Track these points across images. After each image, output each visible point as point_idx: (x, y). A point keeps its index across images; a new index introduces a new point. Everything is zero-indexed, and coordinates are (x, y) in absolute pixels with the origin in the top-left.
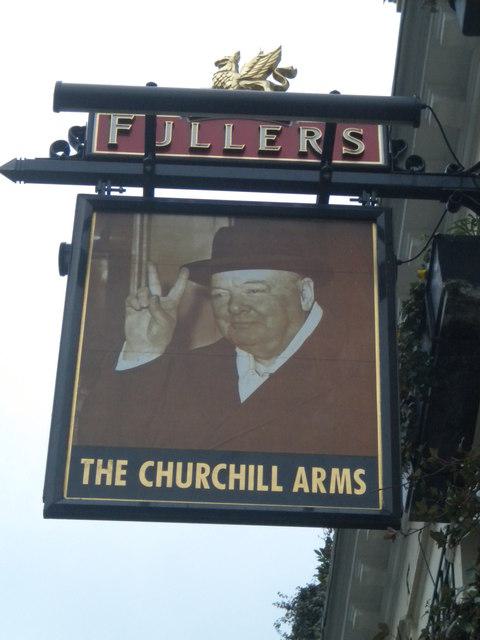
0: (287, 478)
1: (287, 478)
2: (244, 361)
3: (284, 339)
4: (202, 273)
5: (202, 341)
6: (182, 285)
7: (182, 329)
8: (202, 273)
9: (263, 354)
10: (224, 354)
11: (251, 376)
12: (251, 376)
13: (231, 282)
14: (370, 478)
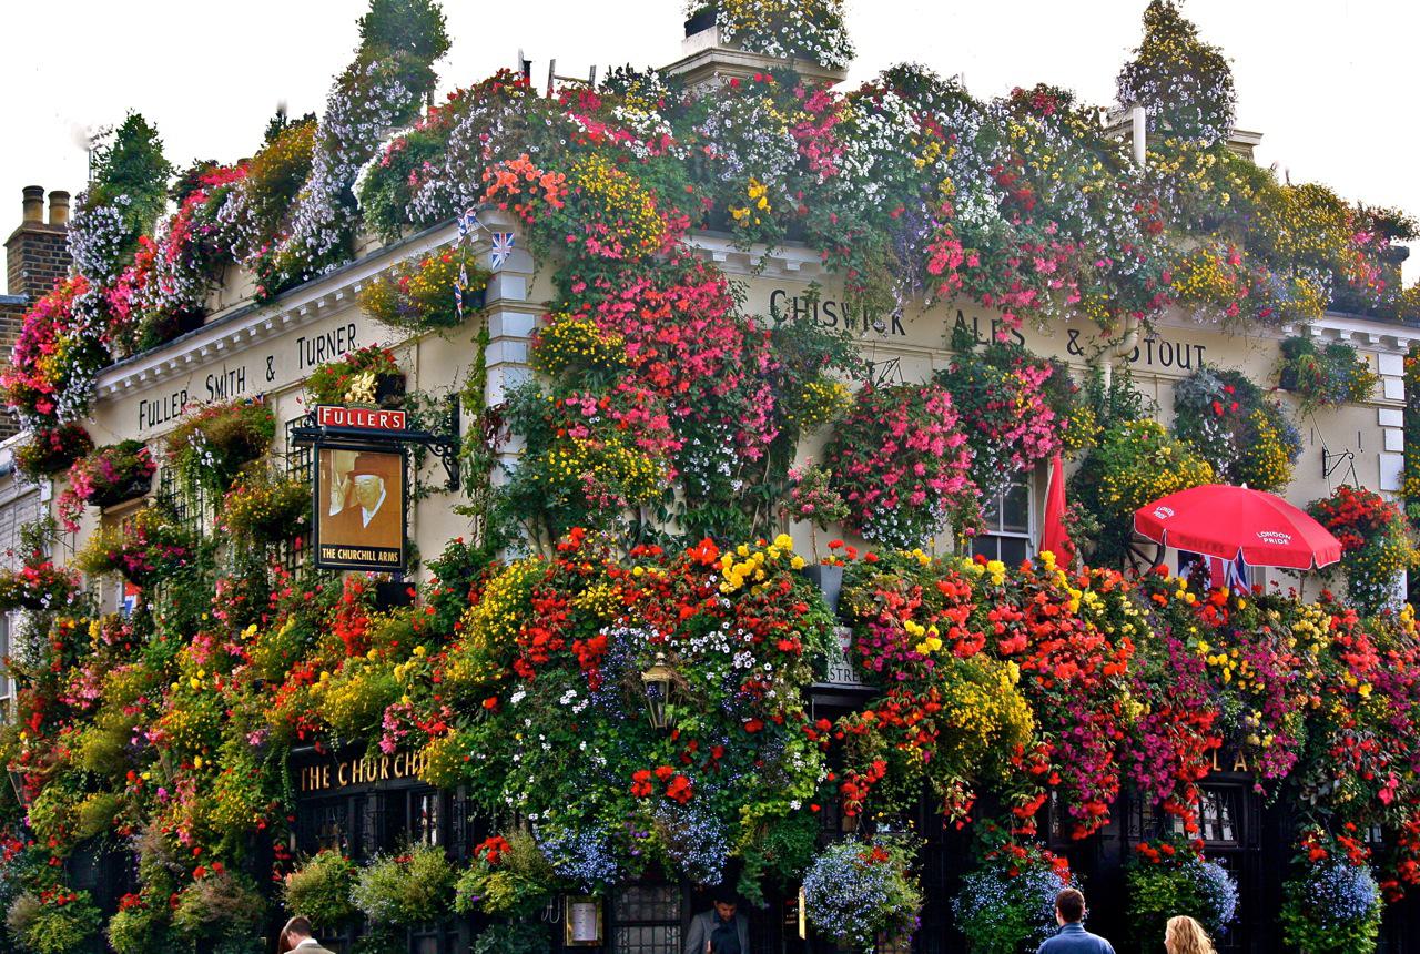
0: (377, 557)
1: (377, 557)
3: (375, 503)
4: (352, 476)
5: (352, 505)
6: (346, 481)
7: (347, 499)
8: (352, 476)
10: (358, 509)
11: (367, 516)
12: (367, 516)
13: (360, 479)
14: (399, 556)
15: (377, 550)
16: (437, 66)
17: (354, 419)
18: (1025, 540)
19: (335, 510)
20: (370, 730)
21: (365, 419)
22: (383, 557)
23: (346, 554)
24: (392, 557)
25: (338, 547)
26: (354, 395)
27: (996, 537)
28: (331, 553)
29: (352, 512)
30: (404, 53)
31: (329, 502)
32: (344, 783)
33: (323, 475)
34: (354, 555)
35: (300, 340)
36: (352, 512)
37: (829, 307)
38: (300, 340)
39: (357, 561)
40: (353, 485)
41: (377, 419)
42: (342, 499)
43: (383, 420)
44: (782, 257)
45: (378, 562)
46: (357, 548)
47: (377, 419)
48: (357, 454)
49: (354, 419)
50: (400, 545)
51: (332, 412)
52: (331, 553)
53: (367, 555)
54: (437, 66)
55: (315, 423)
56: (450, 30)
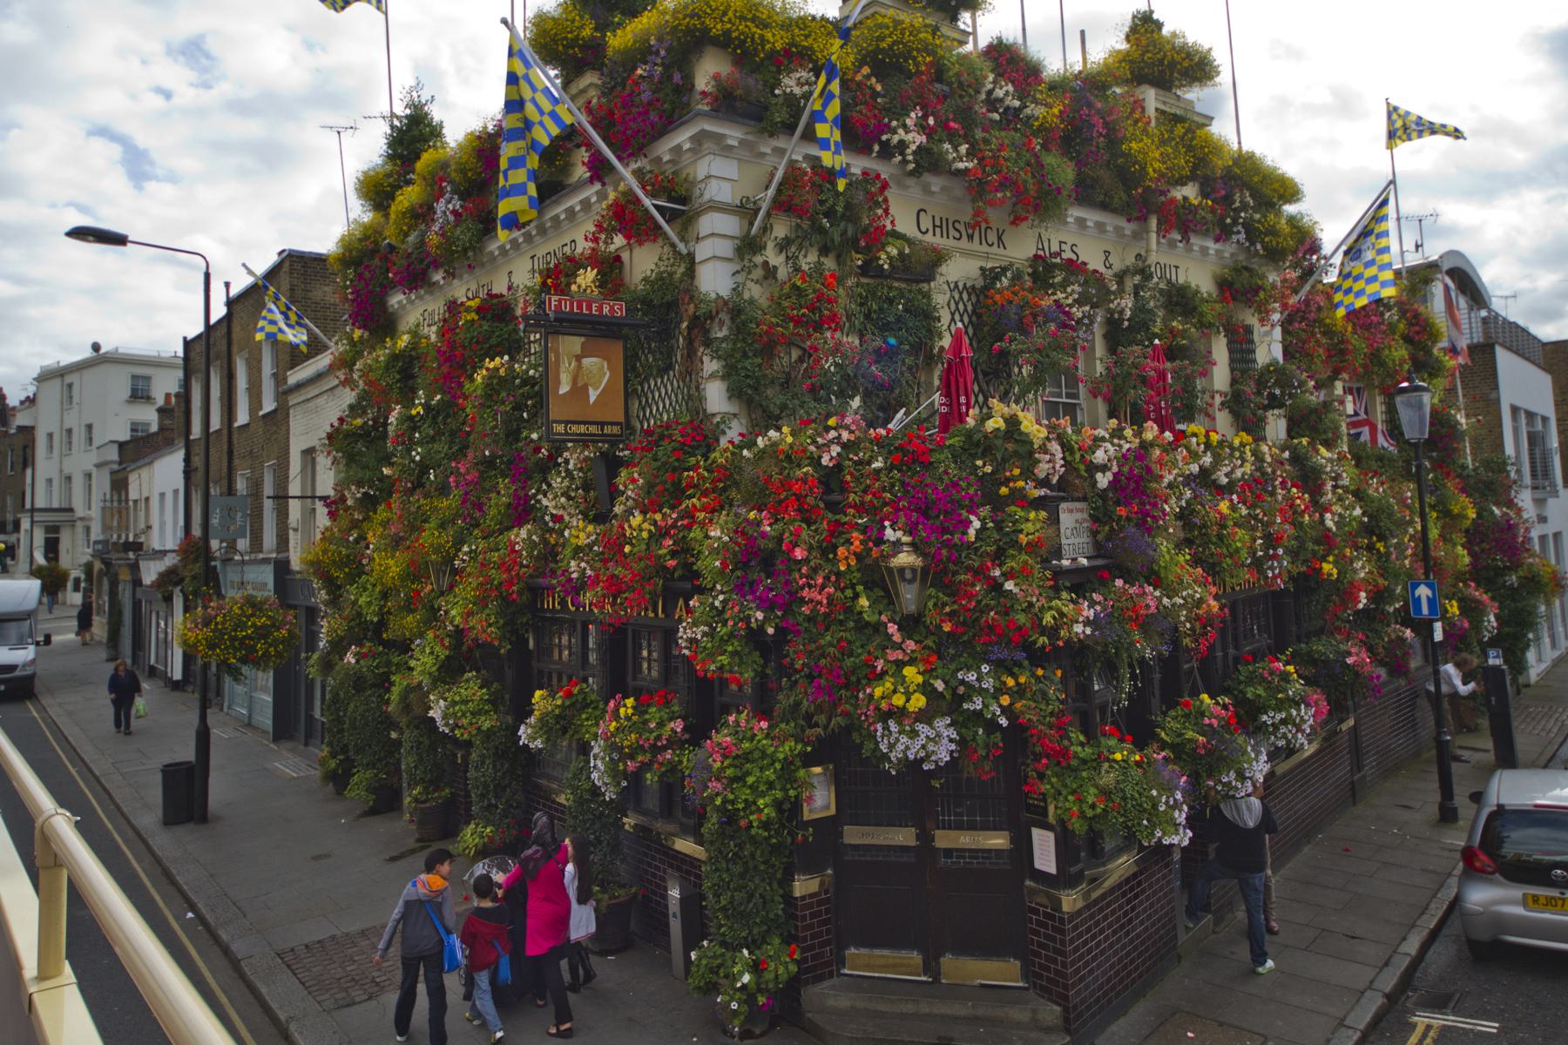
2: (591, 390)
4: (579, 358)
6: (574, 364)
8: (579, 358)
9: (596, 389)
10: (585, 388)
11: (593, 395)
12: (593, 395)
13: (586, 361)
15: (602, 424)
16: (1091, 267)
17: (580, 307)
18: (1075, 404)
19: (564, 389)
20: (584, 968)
21: (589, 308)
22: (607, 430)
23: (575, 428)
24: (616, 430)
25: (567, 423)
26: (579, 287)
27: (1058, 403)
28: (560, 428)
29: (579, 391)
30: (1099, 105)
31: (558, 383)
32: (573, 609)
33: (552, 357)
34: (582, 429)
35: (532, 257)
36: (579, 391)
37: (957, 225)
38: (532, 257)
39: (585, 435)
40: (579, 367)
41: (600, 309)
42: (570, 378)
43: (606, 310)
44: (1536, 541)
45: (603, 435)
46: (585, 423)
47: (600, 309)
48: (583, 339)
49: (580, 307)
50: (621, 419)
51: (560, 301)
52: (560, 428)
53: (593, 429)
54: (1091, 267)
55: (544, 310)
56: (1128, 22)
